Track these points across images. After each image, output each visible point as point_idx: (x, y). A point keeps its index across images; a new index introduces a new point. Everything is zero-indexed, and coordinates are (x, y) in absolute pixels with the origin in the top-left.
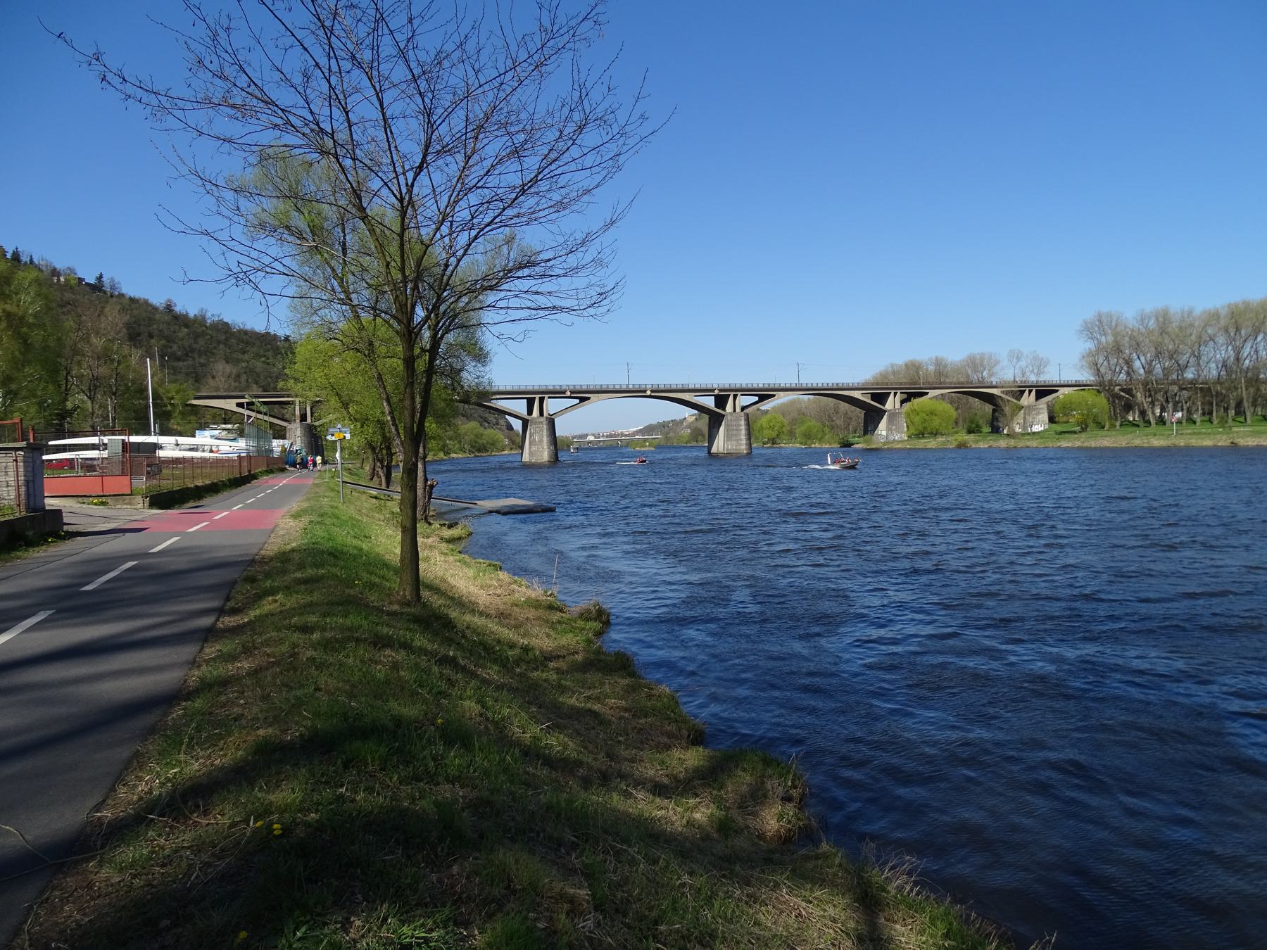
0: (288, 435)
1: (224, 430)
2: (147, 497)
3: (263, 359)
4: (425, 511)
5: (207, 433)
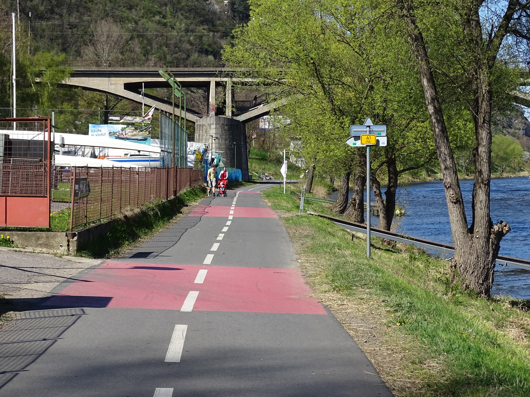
0: (196, 135)
1: (128, 124)
2: (74, 235)
3: (157, 18)
4: (486, 278)
5: (105, 128)
